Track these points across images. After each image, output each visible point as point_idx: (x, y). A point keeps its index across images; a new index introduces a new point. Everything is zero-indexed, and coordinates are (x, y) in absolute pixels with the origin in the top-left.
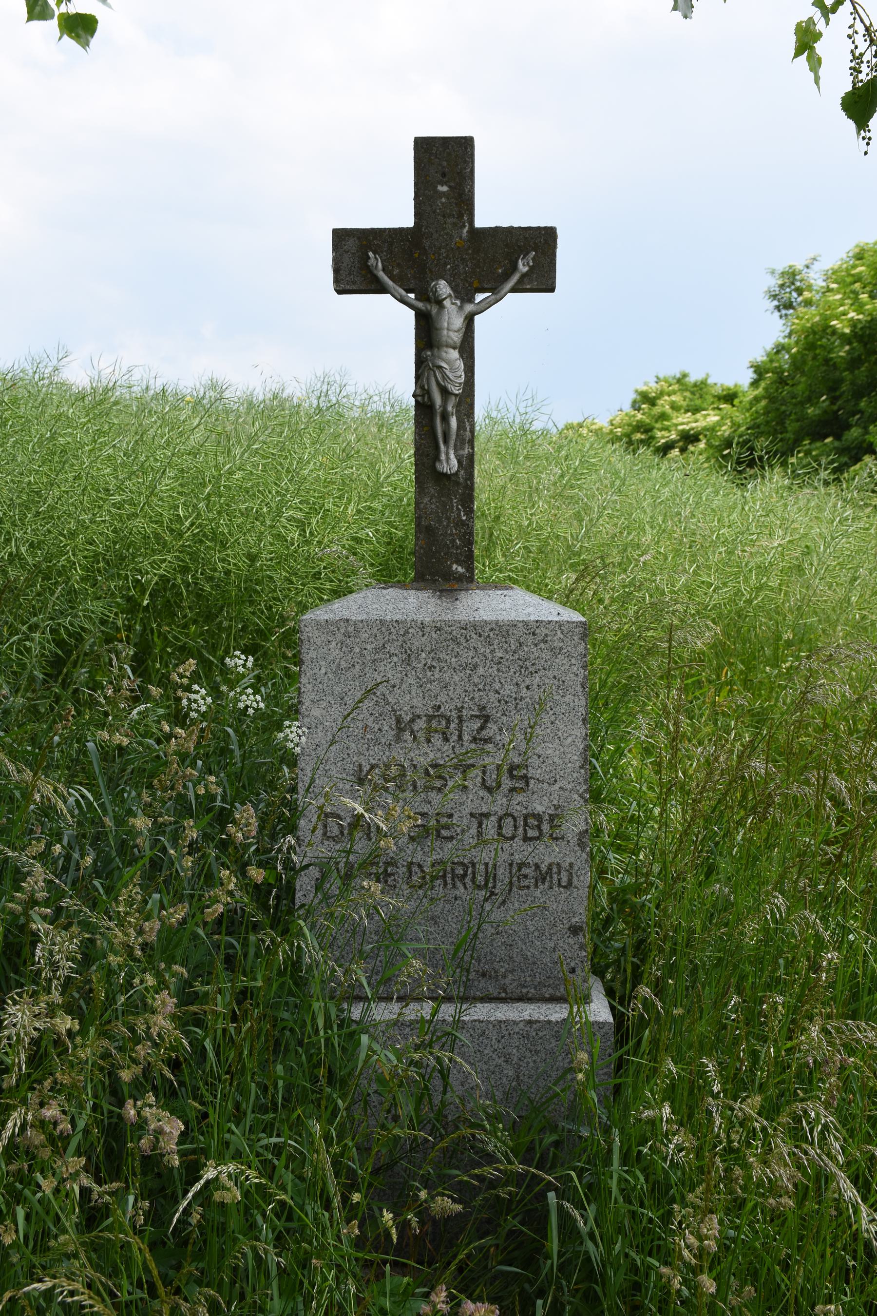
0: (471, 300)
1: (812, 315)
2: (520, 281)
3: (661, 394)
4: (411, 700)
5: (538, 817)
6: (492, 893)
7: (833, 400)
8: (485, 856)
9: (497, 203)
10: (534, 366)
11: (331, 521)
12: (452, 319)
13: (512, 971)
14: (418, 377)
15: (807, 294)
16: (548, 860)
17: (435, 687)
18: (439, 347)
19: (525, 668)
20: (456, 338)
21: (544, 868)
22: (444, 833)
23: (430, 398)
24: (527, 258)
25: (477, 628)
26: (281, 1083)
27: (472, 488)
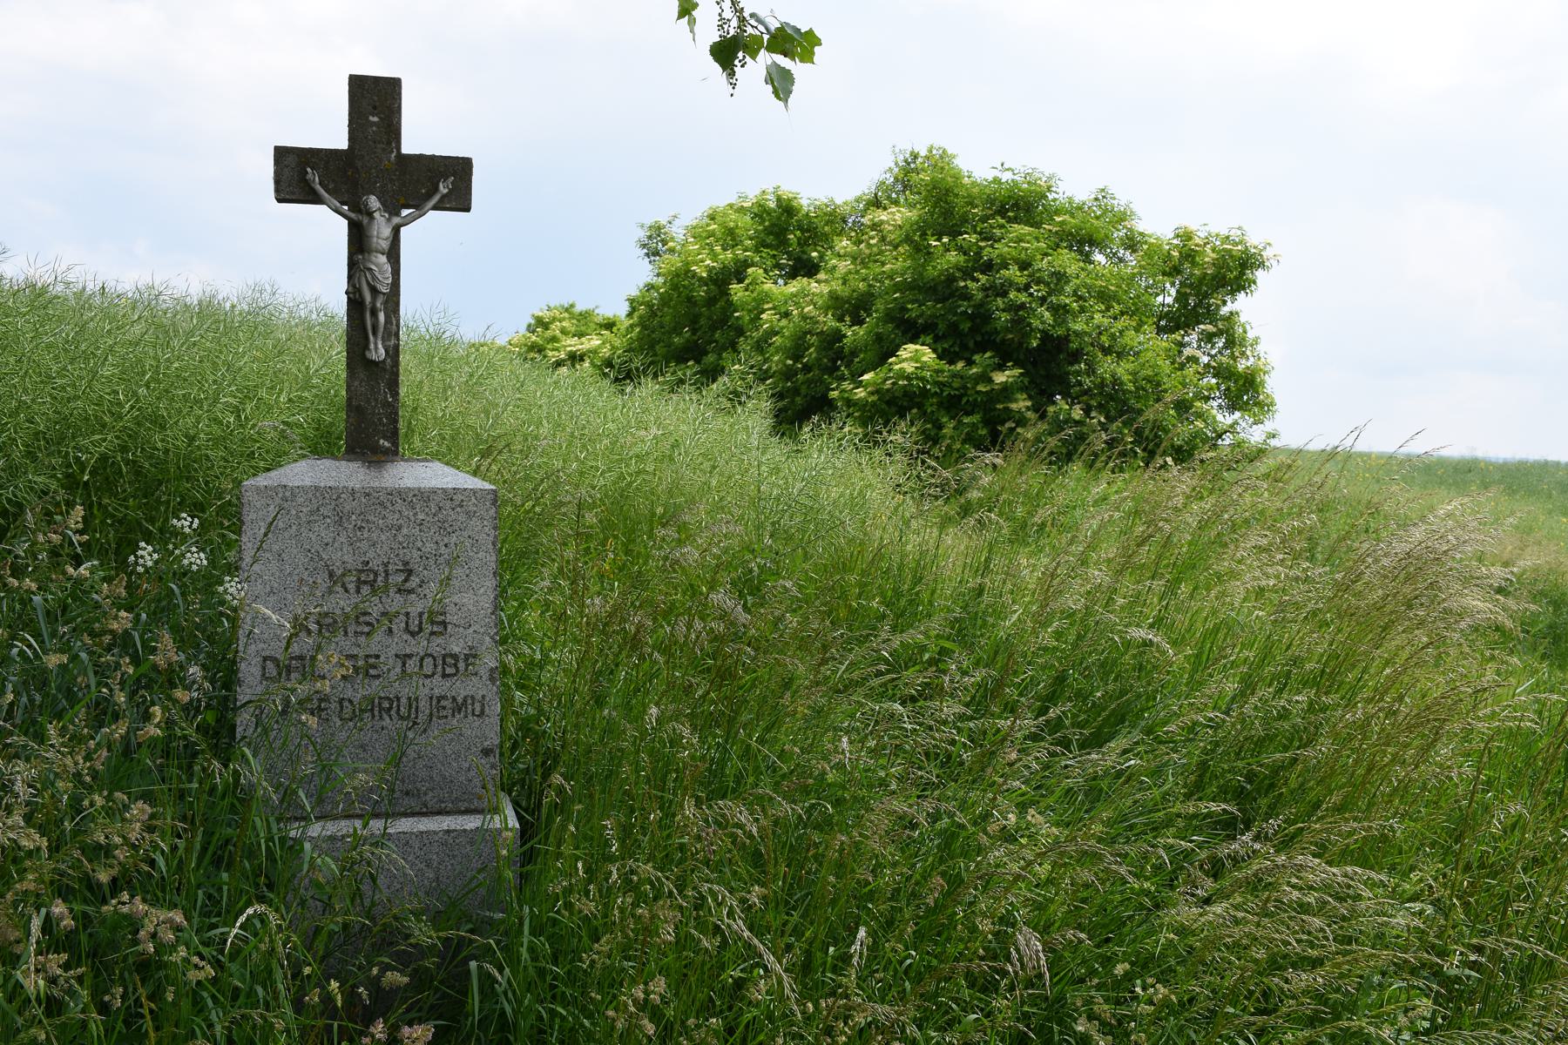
0: (398, 214)
1: (675, 262)
2: (441, 200)
3: (554, 319)
4: (343, 557)
5: (455, 657)
6: (415, 723)
7: (694, 331)
8: (405, 692)
9: (421, 134)
10: (452, 280)
11: (266, 408)
12: (381, 229)
13: (432, 789)
14: (350, 277)
15: (671, 244)
16: (463, 693)
17: (364, 545)
18: (370, 251)
19: (444, 528)
20: (385, 245)
21: (460, 700)
22: (372, 672)
23: (361, 295)
24: (446, 183)
25: (401, 494)
26: (225, 888)
27: (397, 374)
